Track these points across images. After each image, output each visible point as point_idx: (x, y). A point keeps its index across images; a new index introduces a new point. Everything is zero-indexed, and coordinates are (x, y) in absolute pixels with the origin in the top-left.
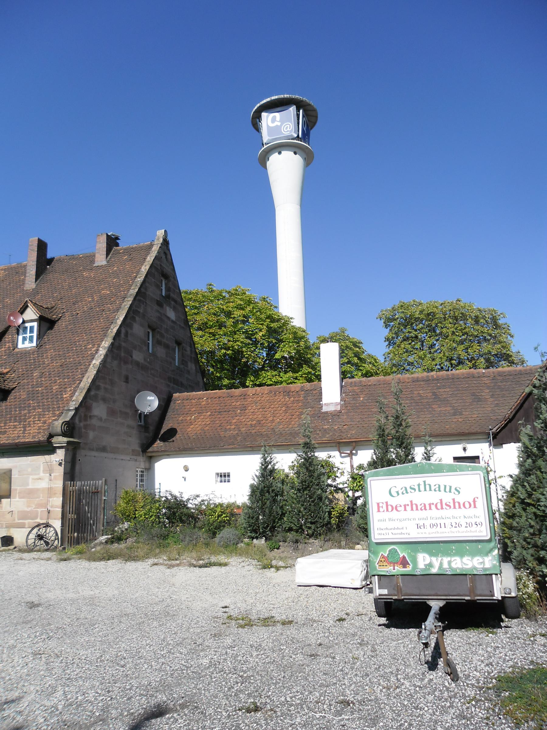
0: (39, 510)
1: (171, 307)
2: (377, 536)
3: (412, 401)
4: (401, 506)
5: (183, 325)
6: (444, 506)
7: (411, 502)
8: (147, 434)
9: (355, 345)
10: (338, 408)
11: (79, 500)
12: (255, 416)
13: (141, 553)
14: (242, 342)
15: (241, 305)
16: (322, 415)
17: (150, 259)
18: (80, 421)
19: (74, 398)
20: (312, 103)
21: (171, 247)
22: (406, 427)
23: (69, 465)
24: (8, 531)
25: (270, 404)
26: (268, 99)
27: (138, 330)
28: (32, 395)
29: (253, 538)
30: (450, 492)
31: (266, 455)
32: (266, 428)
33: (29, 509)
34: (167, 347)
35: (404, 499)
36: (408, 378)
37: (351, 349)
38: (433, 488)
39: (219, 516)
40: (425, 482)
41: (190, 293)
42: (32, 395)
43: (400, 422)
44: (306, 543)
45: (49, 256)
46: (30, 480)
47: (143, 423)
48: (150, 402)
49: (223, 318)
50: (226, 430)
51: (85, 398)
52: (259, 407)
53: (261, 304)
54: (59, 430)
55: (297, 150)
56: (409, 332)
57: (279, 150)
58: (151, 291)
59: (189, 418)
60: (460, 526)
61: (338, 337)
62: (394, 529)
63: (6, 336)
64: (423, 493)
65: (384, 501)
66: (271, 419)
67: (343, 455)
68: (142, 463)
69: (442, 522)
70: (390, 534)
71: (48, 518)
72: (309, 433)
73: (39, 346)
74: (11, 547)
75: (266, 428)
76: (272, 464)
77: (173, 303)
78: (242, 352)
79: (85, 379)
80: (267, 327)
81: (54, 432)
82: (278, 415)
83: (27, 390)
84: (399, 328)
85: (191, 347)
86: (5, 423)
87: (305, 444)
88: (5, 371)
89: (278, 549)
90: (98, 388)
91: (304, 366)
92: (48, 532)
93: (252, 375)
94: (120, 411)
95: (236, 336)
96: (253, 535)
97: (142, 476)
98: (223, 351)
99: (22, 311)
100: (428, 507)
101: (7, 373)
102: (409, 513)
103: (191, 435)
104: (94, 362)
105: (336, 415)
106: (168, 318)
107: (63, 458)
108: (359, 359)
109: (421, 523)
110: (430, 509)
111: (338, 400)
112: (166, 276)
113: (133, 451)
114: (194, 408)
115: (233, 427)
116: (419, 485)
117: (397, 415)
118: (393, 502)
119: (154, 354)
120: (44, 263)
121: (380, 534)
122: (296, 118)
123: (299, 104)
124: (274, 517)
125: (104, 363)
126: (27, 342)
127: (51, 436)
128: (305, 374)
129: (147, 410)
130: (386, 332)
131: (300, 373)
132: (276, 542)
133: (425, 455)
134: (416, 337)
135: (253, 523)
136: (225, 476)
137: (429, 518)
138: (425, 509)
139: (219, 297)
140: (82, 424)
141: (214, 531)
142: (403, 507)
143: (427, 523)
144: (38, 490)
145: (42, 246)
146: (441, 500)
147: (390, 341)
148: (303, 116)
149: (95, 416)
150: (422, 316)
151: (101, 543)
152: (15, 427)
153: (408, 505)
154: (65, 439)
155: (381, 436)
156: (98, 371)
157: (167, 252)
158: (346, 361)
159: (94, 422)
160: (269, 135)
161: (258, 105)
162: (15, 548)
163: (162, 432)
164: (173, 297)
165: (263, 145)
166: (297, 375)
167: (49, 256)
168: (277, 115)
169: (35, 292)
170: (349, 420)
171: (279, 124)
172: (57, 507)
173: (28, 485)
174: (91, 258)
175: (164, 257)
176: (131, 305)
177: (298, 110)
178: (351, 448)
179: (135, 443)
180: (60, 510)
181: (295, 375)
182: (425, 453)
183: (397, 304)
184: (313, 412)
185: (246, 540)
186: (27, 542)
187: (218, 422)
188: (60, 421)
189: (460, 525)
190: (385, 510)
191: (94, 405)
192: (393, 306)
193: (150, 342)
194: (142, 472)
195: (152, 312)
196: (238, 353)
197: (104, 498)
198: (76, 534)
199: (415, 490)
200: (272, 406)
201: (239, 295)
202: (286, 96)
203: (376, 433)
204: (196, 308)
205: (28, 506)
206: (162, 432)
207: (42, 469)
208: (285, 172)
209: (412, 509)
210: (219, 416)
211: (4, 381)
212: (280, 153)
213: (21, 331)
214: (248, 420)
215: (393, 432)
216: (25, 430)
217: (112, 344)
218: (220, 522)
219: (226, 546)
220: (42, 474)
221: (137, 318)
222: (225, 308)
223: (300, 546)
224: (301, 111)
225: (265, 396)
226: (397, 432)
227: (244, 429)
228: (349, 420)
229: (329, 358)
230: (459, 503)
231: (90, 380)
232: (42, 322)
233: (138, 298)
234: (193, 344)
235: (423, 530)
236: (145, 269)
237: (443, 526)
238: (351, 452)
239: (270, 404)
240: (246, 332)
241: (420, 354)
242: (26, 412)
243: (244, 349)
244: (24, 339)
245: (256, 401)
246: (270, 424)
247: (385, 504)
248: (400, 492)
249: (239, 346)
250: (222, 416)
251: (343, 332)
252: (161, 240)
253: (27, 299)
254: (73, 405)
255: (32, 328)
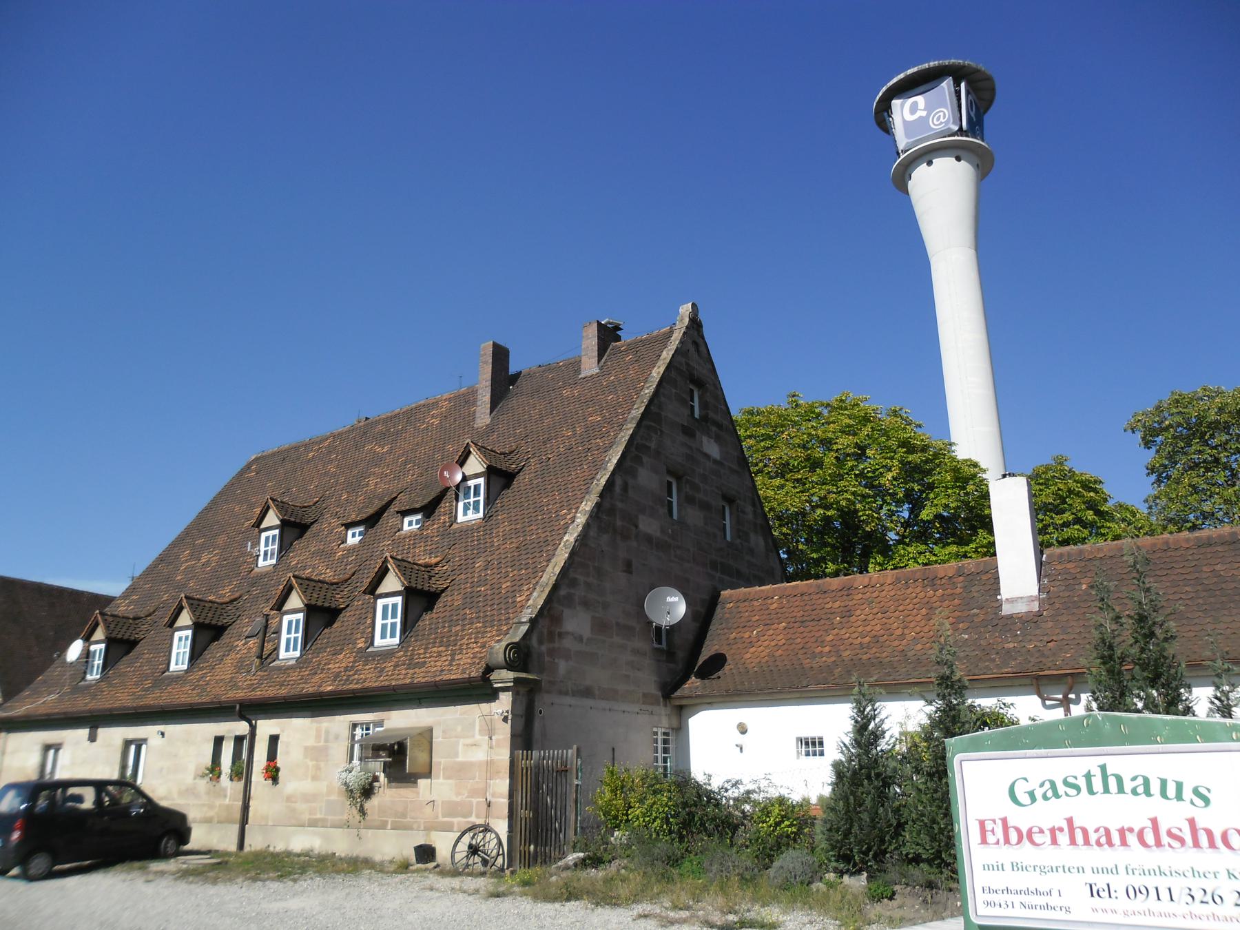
0: (475, 801)
1: (710, 437)
2: (982, 910)
3: (1199, 588)
4: (1041, 831)
5: (735, 467)
6: (1165, 839)
7: (1070, 821)
8: (672, 666)
9: (1086, 486)
10: (1035, 607)
11: (537, 786)
12: (869, 628)
13: (623, 891)
14: (854, 493)
15: (849, 426)
16: (1001, 623)
17: (667, 355)
18: (541, 642)
19: (530, 602)
20: (981, 67)
21: (706, 331)
22: (1166, 640)
23: (521, 722)
24: (428, 835)
25: (896, 604)
26: (902, 76)
27: (648, 478)
28: (470, 600)
29: (841, 874)
30: (1179, 797)
31: (864, 703)
32: (889, 650)
33: (459, 799)
34: (705, 506)
35: (1048, 814)
36: (1187, 540)
37: (1078, 494)
38: (1128, 786)
39: (778, 824)
40: (1103, 768)
41: (759, 413)
42: (470, 600)
43: (1150, 628)
44: (951, 890)
45: (513, 369)
46: (460, 748)
47: (664, 645)
48: (673, 607)
49: (818, 453)
50: (814, 655)
51: (548, 601)
52: (876, 610)
53: (887, 421)
54: (500, 658)
55: (959, 153)
56: (1200, 452)
57: (928, 158)
58: (673, 411)
59: (746, 635)
60: (1217, 899)
61: (1050, 474)
62: (1028, 892)
63: (442, 505)
64: (1100, 798)
65: (998, 816)
66: (899, 632)
67: (1048, 703)
68: (663, 720)
69: (1163, 883)
70: (1017, 905)
71: (487, 816)
72: (949, 657)
73: (487, 517)
74: (433, 864)
75: (889, 650)
76: (877, 720)
77: (714, 429)
78: (856, 511)
79: (549, 569)
80: (901, 462)
81: (493, 662)
82: (912, 625)
83: (463, 592)
84: (1174, 445)
85: (754, 505)
86: (426, 648)
87: (942, 678)
88: (434, 561)
89: (891, 898)
90: (573, 583)
91: (980, 531)
92: (487, 839)
93: (878, 553)
94: (618, 624)
95: (842, 483)
96: (841, 866)
97: (665, 742)
98: (820, 511)
99: (462, 462)
100: (1116, 838)
101: (437, 564)
102: (1065, 853)
103: (750, 666)
104: (566, 538)
105: (1029, 621)
106: (707, 456)
107: (509, 708)
108: (1098, 513)
109: (1100, 881)
110: (1124, 842)
111: (1033, 590)
112: (700, 384)
113: (645, 695)
114: (756, 617)
115: (827, 649)
116: (1088, 777)
117: (1139, 614)
118: (1021, 818)
119: (681, 522)
120: (504, 381)
121: (989, 904)
122: (955, 99)
123: (957, 74)
124: (881, 830)
125: (583, 538)
126: (470, 512)
127: (489, 669)
128: (982, 547)
129: (666, 621)
130: (1149, 456)
131: (973, 545)
132: (886, 884)
133: (1217, 702)
134: (1217, 460)
135: (837, 841)
136: (814, 744)
137: (1122, 870)
138: (1110, 843)
139: (811, 414)
140: (544, 648)
141: (768, 851)
142: (1048, 833)
143: (1119, 883)
144: (471, 764)
145: (500, 355)
146: (1154, 822)
147: (1158, 473)
148: (968, 93)
149: (567, 633)
150: (1224, 418)
151: (567, 868)
152: (439, 654)
153: (1061, 830)
154: (511, 675)
155: (1106, 659)
156: (572, 554)
157: (699, 341)
158: (1071, 518)
159: (567, 643)
160: (907, 135)
161: (884, 89)
162: (438, 866)
163: (700, 661)
164: (716, 418)
165: (898, 154)
166: (967, 548)
167: (513, 369)
168: (920, 100)
169: (490, 429)
170: (1058, 631)
171: (924, 114)
172: (501, 796)
173: (456, 755)
174: (576, 365)
175: (692, 349)
176: (632, 437)
177: (957, 83)
178: (1064, 688)
179: (648, 680)
180: (505, 801)
181: (963, 550)
182: (1216, 698)
183: (1166, 399)
184: (982, 617)
185: (831, 876)
186: (453, 857)
187: (799, 640)
188: (504, 644)
189: (1217, 899)
190: (1002, 841)
191: (567, 612)
192: (1156, 403)
193: (675, 500)
194: (664, 734)
195: (675, 447)
196: (848, 516)
197: (576, 782)
198: (532, 847)
199: (1078, 789)
200: (901, 608)
201: (846, 409)
202: (932, 64)
203: (1095, 655)
204: (769, 438)
205: (458, 794)
206: (700, 661)
207: (477, 728)
208: (942, 197)
209: (1073, 842)
210: (802, 629)
211: (430, 578)
212: (930, 163)
213: (461, 495)
214: (856, 635)
215: (1134, 651)
216: (453, 660)
217: (598, 506)
218: (780, 836)
219: (785, 887)
220: (478, 737)
221: (645, 459)
222: (820, 433)
223: (942, 895)
224: (963, 85)
225: (887, 589)
226: (1142, 650)
227: (848, 653)
228: (1058, 631)
229: (1010, 506)
230: (1209, 833)
231: (557, 570)
232: (493, 478)
233: (645, 423)
234: (757, 502)
235: (1105, 902)
236: (657, 372)
237: (1164, 895)
238: (1066, 697)
239: (896, 604)
240: (862, 475)
241: (1225, 493)
242: (458, 628)
243: (859, 506)
244: (466, 508)
245: (872, 598)
246: (897, 643)
247: (999, 823)
248: (1039, 793)
249: (848, 500)
250: (808, 629)
251: (1061, 464)
252: (687, 321)
253: (469, 440)
254: (527, 614)
255: (477, 487)
